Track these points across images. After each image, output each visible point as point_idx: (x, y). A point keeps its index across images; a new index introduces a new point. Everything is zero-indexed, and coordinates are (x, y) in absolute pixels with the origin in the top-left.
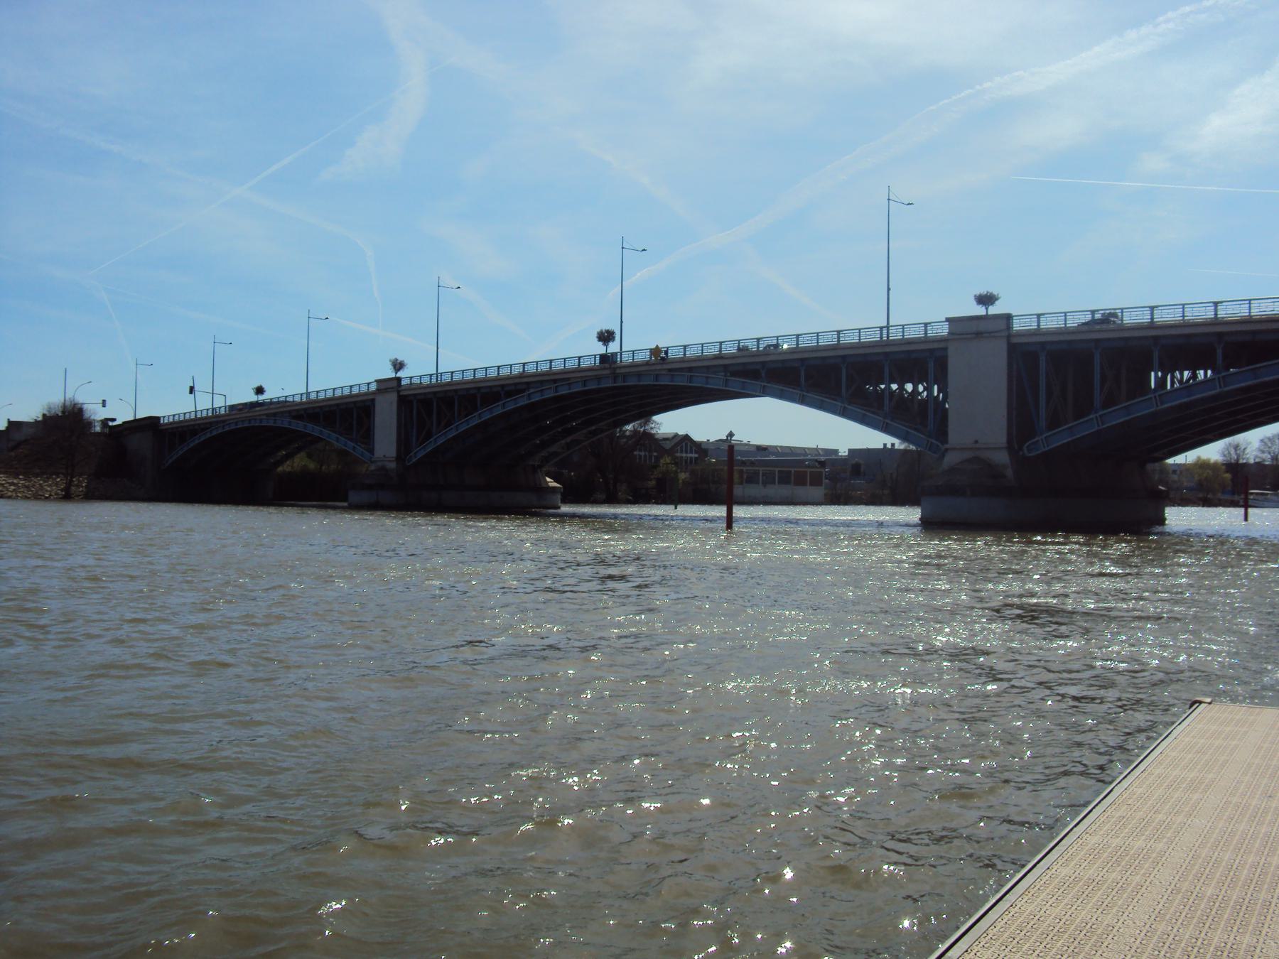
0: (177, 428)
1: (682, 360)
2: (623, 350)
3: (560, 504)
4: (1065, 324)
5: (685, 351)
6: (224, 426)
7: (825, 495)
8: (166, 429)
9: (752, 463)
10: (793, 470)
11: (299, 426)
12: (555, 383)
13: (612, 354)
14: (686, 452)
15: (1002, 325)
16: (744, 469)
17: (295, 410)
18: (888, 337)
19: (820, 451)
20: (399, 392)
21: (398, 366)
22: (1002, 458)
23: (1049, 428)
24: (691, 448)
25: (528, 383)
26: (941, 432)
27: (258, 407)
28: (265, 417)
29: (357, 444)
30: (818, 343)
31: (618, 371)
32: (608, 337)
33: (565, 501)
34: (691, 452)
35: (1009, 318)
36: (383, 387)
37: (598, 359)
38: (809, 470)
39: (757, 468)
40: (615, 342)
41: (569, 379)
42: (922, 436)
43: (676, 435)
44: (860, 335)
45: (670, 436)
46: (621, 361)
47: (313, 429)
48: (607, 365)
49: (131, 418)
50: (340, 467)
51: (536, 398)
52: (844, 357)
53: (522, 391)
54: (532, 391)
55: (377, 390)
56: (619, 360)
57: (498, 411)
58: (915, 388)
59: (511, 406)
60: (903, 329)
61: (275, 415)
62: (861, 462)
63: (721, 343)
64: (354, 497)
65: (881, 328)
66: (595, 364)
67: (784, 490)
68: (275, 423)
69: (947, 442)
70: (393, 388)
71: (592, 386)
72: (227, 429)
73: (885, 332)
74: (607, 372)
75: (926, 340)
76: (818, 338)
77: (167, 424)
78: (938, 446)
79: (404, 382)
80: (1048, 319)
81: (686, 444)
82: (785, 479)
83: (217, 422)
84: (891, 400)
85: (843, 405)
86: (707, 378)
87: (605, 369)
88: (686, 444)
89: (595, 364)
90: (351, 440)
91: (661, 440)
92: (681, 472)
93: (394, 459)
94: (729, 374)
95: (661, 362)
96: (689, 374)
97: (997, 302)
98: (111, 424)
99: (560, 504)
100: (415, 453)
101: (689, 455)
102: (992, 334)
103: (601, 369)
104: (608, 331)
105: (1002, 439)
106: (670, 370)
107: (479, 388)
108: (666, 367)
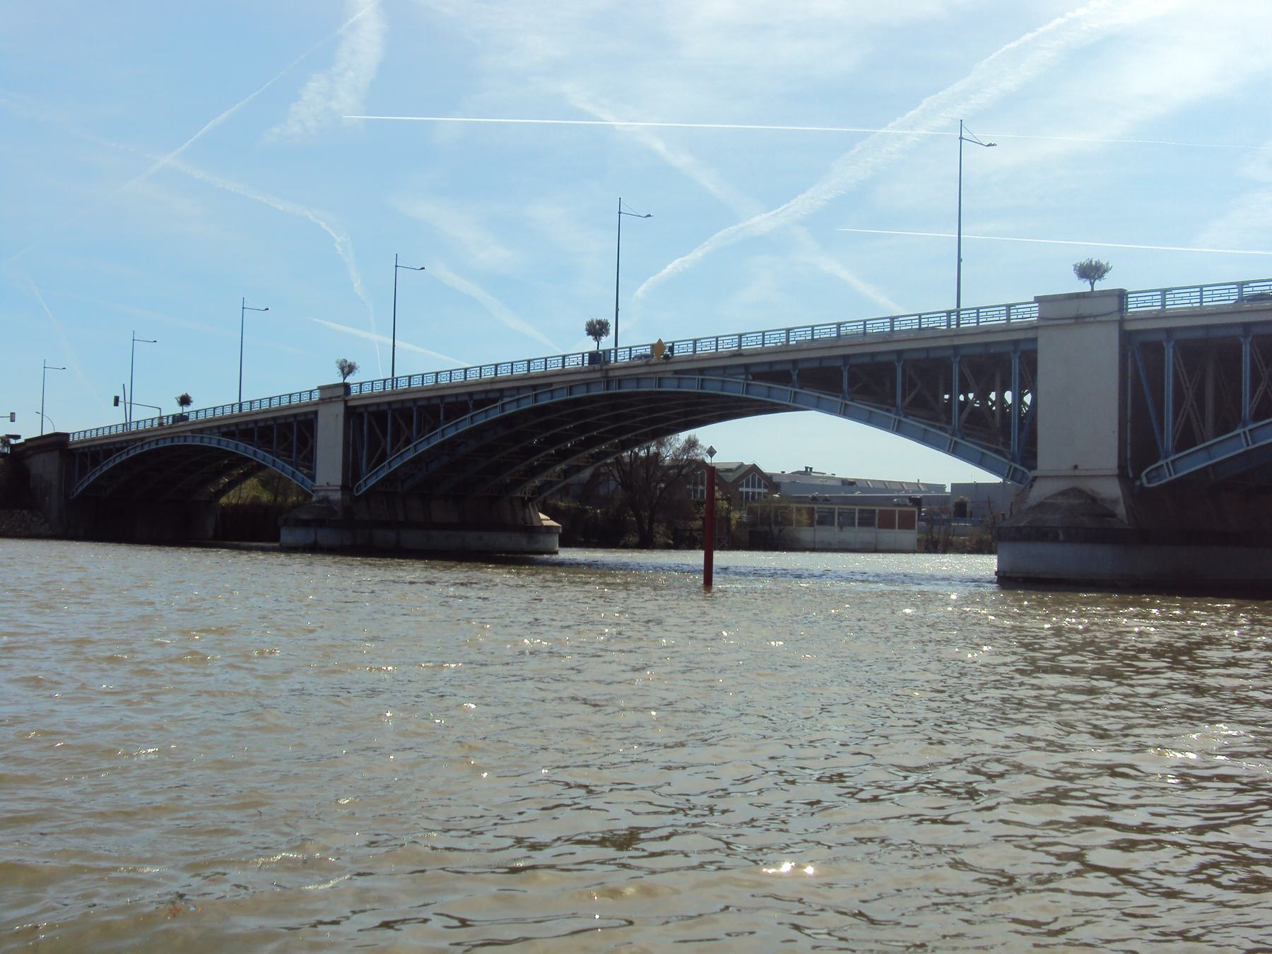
0: (89, 447)
1: (690, 359)
2: (619, 346)
3: (557, 548)
4: (1201, 302)
5: (1008, 314)
6: (142, 445)
7: (918, 540)
8: (77, 449)
9: (826, 500)
10: (877, 509)
11: (229, 445)
12: (535, 390)
13: (604, 352)
14: (753, 486)
15: (1113, 305)
16: (816, 506)
17: (224, 425)
18: (958, 324)
19: (904, 485)
20: (346, 402)
21: (347, 369)
22: (1111, 490)
23: (1179, 447)
24: (759, 481)
25: (501, 391)
26: (1029, 455)
27: (182, 421)
28: (189, 434)
29: (297, 469)
30: (978, 323)
31: (611, 374)
32: (601, 329)
33: (566, 542)
34: (759, 487)
35: (1121, 295)
36: (328, 394)
37: (586, 358)
38: (897, 509)
39: (832, 506)
40: (609, 337)
41: (551, 384)
42: (1003, 460)
43: (741, 465)
44: (1201, 295)
45: (734, 467)
46: (616, 361)
47: (245, 449)
48: (597, 367)
49: (39, 434)
50: (300, 498)
51: (511, 410)
52: (1169, 331)
53: (495, 400)
54: (506, 400)
55: (321, 399)
56: (613, 359)
57: (465, 426)
58: (966, 397)
59: (480, 420)
60: (1201, 291)
61: (201, 431)
62: (966, 499)
63: (740, 336)
64: (287, 536)
65: (949, 313)
66: (583, 364)
67: (866, 534)
68: (201, 442)
69: (1034, 467)
70: (338, 397)
71: (580, 393)
72: (146, 448)
73: (954, 317)
74: (598, 375)
75: (1008, 328)
76: (978, 316)
77: (77, 443)
78: (1024, 472)
79: (355, 391)
80: (1176, 296)
81: (754, 477)
82: (866, 520)
83: (135, 441)
84: (961, 411)
85: (898, 418)
86: (723, 381)
87: (594, 371)
88: (754, 477)
89: (583, 364)
90: (290, 464)
91: (722, 472)
92: (734, 510)
93: (339, 488)
94: (750, 377)
95: (665, 361)
96: (701, 377)
97: (1106, 275)
98: (13, 442)
99: (557, 548)
100: (365, 481)
101: (757, 490)
102: (1099, 319)
103: (589, 372)
104: (599, 322)
105: (1110, 462)
106: (676, 372)
107: (442, 397)
108: (670, 367)
